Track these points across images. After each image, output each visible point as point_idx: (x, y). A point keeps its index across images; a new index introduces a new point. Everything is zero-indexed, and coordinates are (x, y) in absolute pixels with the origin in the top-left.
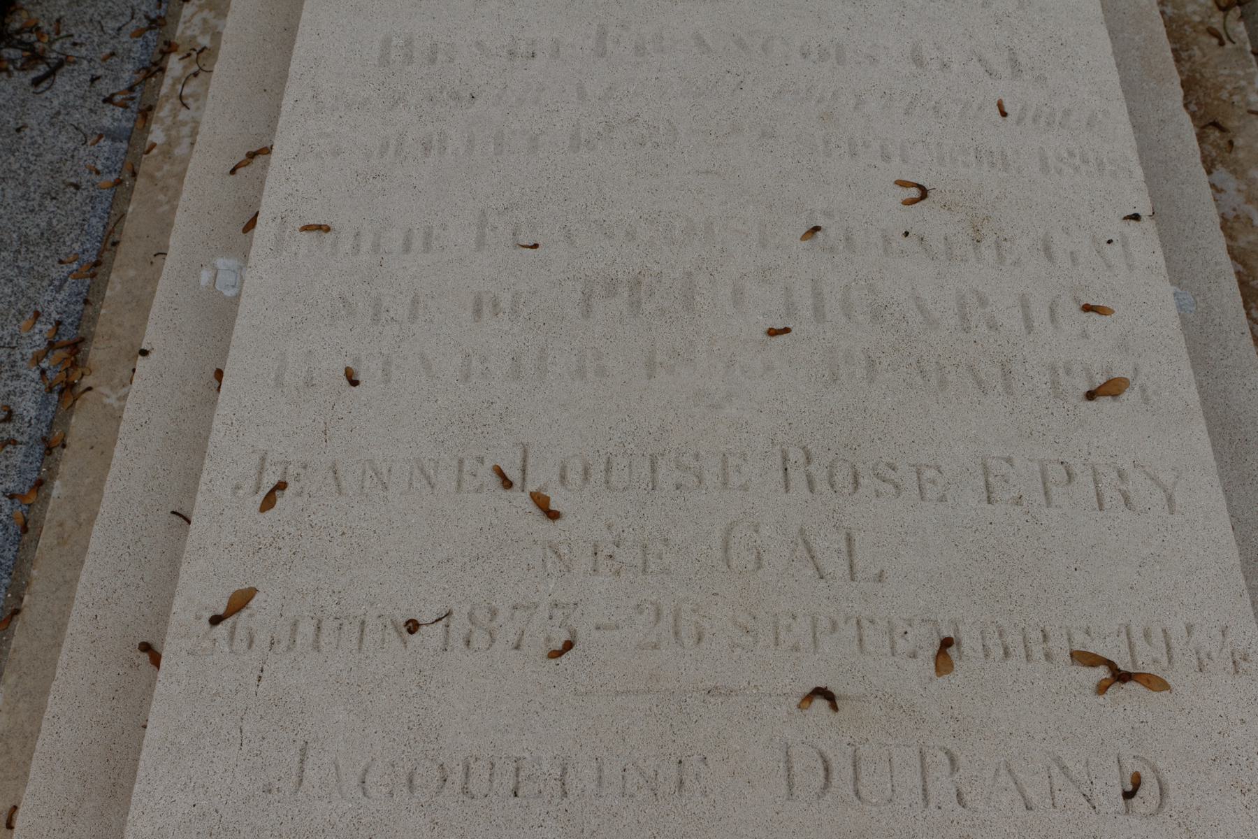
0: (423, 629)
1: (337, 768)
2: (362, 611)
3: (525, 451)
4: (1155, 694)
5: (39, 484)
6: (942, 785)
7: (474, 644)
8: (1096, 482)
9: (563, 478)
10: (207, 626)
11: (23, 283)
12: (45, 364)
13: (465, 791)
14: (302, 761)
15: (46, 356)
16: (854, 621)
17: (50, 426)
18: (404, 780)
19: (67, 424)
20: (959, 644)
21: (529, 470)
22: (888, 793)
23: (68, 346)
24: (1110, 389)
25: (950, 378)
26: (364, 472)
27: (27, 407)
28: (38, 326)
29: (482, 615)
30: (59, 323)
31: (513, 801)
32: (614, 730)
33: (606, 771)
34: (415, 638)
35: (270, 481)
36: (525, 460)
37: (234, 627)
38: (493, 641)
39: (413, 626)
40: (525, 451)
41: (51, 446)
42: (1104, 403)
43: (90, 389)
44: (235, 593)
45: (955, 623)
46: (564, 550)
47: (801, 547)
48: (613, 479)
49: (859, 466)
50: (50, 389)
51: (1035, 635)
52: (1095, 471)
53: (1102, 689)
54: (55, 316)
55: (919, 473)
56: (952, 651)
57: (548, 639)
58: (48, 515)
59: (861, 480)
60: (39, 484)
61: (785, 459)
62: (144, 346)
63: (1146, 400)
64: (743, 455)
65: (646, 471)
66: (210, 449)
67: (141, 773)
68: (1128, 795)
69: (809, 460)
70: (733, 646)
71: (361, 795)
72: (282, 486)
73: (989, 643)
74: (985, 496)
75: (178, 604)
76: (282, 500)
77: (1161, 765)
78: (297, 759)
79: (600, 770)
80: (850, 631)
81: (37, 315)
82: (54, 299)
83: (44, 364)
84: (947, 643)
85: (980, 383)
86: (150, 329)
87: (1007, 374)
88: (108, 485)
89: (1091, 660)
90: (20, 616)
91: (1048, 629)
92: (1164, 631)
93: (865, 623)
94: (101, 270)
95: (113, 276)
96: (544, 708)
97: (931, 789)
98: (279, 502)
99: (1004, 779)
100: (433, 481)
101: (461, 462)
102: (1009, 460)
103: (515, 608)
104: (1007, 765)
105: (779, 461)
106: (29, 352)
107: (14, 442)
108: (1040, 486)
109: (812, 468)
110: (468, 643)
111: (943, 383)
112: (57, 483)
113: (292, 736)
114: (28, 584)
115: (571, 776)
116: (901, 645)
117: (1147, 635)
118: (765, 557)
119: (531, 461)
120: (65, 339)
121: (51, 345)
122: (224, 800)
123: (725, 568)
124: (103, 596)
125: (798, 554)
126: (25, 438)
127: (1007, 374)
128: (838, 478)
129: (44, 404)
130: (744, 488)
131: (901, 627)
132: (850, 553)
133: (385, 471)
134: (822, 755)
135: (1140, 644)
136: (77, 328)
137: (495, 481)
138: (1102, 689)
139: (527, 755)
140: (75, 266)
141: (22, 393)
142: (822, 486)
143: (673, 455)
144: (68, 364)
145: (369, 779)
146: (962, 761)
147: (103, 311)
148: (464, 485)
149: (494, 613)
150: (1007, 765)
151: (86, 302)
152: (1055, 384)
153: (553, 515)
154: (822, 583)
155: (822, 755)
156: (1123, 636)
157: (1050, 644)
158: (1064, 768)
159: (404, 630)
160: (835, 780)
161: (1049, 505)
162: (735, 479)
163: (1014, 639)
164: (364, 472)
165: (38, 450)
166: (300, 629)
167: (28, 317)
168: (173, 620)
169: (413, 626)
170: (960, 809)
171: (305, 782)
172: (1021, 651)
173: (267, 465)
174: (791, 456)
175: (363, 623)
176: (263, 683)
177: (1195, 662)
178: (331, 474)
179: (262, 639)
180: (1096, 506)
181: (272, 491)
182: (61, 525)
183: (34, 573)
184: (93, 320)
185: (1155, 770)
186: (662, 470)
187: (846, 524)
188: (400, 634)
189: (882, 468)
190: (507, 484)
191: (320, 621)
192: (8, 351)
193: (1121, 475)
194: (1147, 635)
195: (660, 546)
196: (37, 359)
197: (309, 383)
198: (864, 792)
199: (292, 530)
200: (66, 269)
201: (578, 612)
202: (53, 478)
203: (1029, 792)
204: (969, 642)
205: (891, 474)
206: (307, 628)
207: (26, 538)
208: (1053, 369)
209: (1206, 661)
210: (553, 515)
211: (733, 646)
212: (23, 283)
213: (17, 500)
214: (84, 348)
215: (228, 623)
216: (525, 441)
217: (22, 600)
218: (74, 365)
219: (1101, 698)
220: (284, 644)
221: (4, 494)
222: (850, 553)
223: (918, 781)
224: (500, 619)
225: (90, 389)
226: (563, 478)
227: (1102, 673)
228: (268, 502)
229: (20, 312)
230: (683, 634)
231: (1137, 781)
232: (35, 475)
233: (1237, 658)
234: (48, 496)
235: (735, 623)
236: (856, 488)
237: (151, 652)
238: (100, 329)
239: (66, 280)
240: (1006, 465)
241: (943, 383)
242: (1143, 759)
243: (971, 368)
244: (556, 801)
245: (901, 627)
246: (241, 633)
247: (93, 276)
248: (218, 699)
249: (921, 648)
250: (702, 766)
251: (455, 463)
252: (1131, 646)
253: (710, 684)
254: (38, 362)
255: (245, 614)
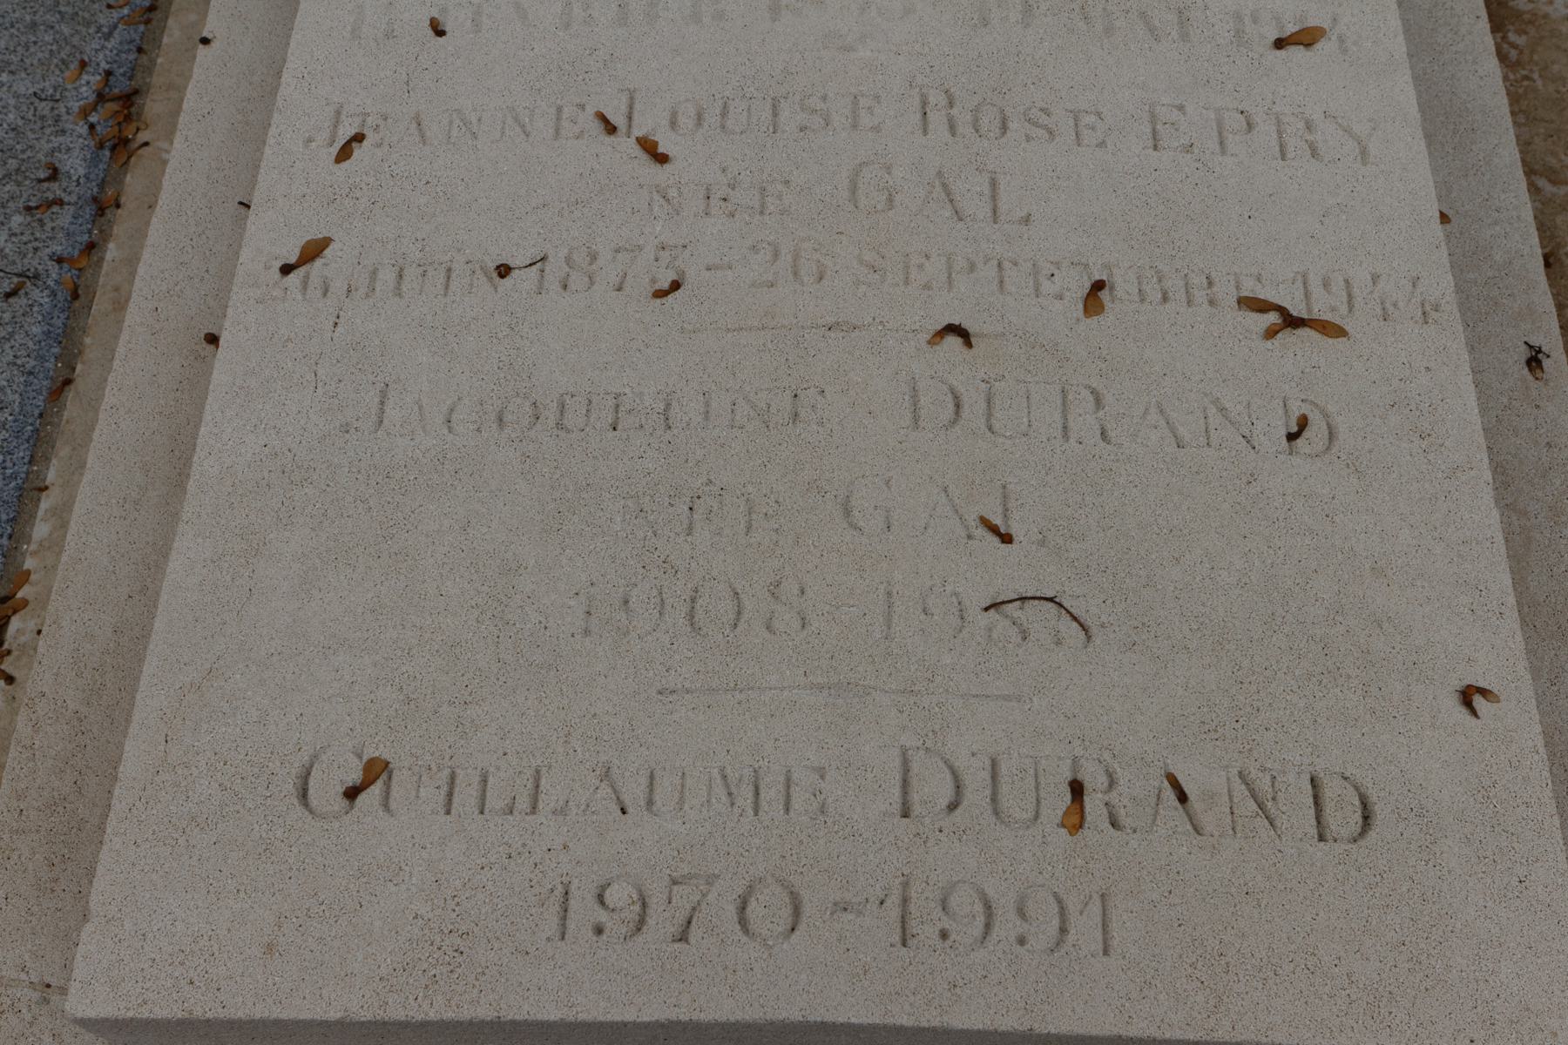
0: (515, 273)
1: (421, 407)
2: (447, 258)
3: (632, 98)
4: (1331, 341)
5: (91, 246)
6: (1084, 420)
7: (572, 286)
8: (1280, 133)
9: (673, 124)
10: (277, 275)
11: (66, 30)
12: (93, 119)
13: (559, 425)
14: (382, 403)
15: (94, 109)
16: (995, 262)
17: (102, 185)
18: (493, 416)
19: (121, 182)
20: (1112, 288)
21: (636, 116)
22: (1024, 428)
23: (119, 98)
24: (1306, 38)
25: (1118, 24)
26: (451, 123)
27: (75, 164)
28: (85, 77)
29: (580, 258)
30: (109, 73)
31: (611, 434)
32: (723, 365)
33: (714, 405)
34: (508, 281)
35: (346, 132)
36: (631, 107)
37: (307, 277)
38: (592, 283)
39: (504, 271)
40: (632, 98)
41: (103, 206)
42: (1295, 53)
43: (146, 144)
44: (308, 242)
45: (1107, 267)
46: (673, 193)
47: (939, 189)
48: (729, 123)
49: (1009, 111)
50: (101, 146)
51: (1198, 280)
52: (1279, 122)
53: (1271, 333)
54: (104, 65)
55: (1076, 120)
56: (1104, 295)
57: (653, 281)
58: (101, 280)
59: (1010, 125)
60: (91, 246)
61: (924, 103)
62: (205, 34)
63: (1345, 51)
64: (877, 98)
65: (767, 114)
66: (280, 103)
67: (207, 417)
68: (1292, 437)
69: (951, 104)
70: (857, 283)
71: (446, 431)
72: (359, 138)
73: (1147, 288)
74: (1150, 143)
75: (245, 255)
76: (358, 152)
77: (1331, 408)
78: (377, 400)
79: (707, 404)
80: (990, 271)
81: (83, 64)
82: (103, 47)
83: (93, 119)
84: (1098, 286)
85: (1152, 30)
86: (211, 16)
87: (1183, 19)
88: (167, 177)
89: (1261, 306)
90: (72, 387)
91: (1213, 274)
92: (1347, 281)
93: (1006, 265)
94: (157, 15)
95: (170, 22)
96: (647, 346)
97: (1071, 424)
98: (356, 153)
99: (1154, 416)
100: (529, 128)
101: (559, 110)
102: (1181, 108)
103: (617, 251)
104: (1159, 406)
105: (917, 101)
106: (76, 106)
107: (60, 202)
108: (1215, 134)
109: (954, 111)
110: (565, 287)
111: (1109, 30)
112: (111, 245)
113: (371, 378)
114: (80, 352)
115: (675, 411)
116: (1046, 286)
117: (1326, 284)
118: (898, 198)
119: (637, 106)
120: (116, 91)
121: (101, 97)
122: (297, 440)
123: (851, 208)
124: (164, 288)
125: (934, 195)
126: (73, 198)
127: (1183, 19)
128: (984, 122)
129: (94, 161)
130: (876, 129)
131: (1047, 269)
132: (994, 198)
133: (474, 120)
134: (953, 391)
135: (1317, 290)
136: (130, 79)
137: (596, 127)
138: (1271, 333)
139: (627, 390)
140: (126, 11)
141: (69, 149)
142: (965, 129)
143: (797, 97)
144: (122, 119)
145: (454, 417)
146: (1108, 399)
147: (159, 61)
148: (563, 132)
149: (594, 257)
150: (1159, 406)
151: (140, 50)
152: (1239, 33)
153: (662, 159)
154: (961, 225)
155: (953, 391)
156: (1299, 284)
157: (1215, 289)
158: (1222, 410)
159: (495, 275)
160: (966, 412)
161: (1223, 152)
162: (866, 120)
163: (1174, 284)
164: (451, 123)
165: (89, 211)
166: (380, 275)
167: (72, 67)
168: (240, 270)
169: (504, 271)
170: (1103, 444)
171: (386, 421)
172: (1182, 295)
173: (343, 117)
174: (931, 99)
175: (449, 270)
176: (339, 329)
177: (1379, 311)
178: (414, 125)
179: (338, 286)
180: (1278, 155)
181: (349, 143)
182: (117, 289)
183: (88, 340)
184: (149, 70)
185: (1326, 416)
186: (785, 114)
187: (991, 168)
188: (490, 279)
189: (1035, 113)
190: (611, 129)
191: (402, 269)
192: (51, 104)
193: (1309, 126)
194: (1326, 284)
195: (780, 187)
196: (84, 113)
197: (390, 35)
198: (997, 426)
199: (372, 180)
200: (115, 14)
201: (687, 252)
202: (106, 241)
203: (1181, 430)
204: (1124, 284)
205: (1044, 119)
206: (387, 276)
207: (77, 304)
208: (1238, 17)
209: (1391, 309)
210: (662, 159)
211: (857, 283)
212: (66, 30)
213: (65, 265)
214: (138, 100)
215: (301, 271)
216: (631, 87)
217: (74, 369)
218: (128, 118)
219: (1269, 343)
220: (362, 291)
221: (51, 258)
222: (994, 198)
223: (1057, 416)
224: (600, 262)
225: (146, 144)
226: (673, 124)
227: (1273, 318)
228: (344, 154)
229: (63, 61)
230: (802, 273)
231: (1303, 423)
232: (86, 237)
233: (1428, 308)
234: (102, 259)
235: (861, 262)
236: (1004, 133)
237: (213, 339)
238: (156, 80)
239: (115, 27)
240: (1176, 112)
241: (1109, 30)
242: (1312, 403)
243: (1143, 15)
244: (659, 433)
245: (1047, 269)
246: (315, 281)
247: (148, 22)
248: (290, 345)
249: (1069, 290)
250: (819, 398)
251: (553, 110)
252: (1307, 295)
253: (831, 320)
254: (86, 116)
255: (318, 263)
